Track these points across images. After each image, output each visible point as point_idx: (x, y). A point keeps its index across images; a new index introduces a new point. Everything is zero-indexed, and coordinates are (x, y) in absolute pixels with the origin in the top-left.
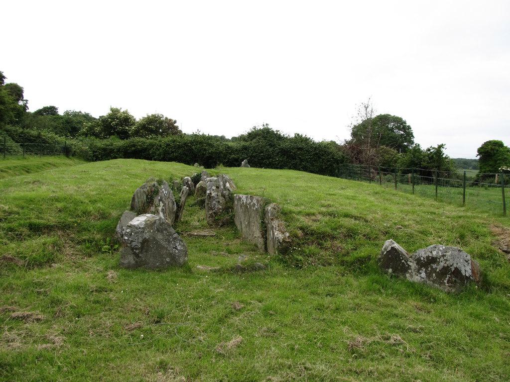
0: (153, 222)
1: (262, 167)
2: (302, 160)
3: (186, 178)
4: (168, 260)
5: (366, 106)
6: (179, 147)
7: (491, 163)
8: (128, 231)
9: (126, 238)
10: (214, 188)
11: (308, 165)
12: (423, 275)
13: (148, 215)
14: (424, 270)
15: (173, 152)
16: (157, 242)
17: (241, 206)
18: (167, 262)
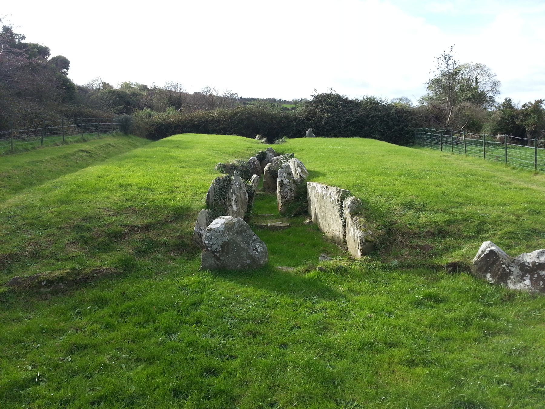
3: (251, 158)
4: (248, 262)
8: (208, 234)
9: (207, 242)
10: (286, 175)
12: (527, 282)
13: (226, 217)
14: (529, 276)
16: (237, 244)
18: (248, 264)
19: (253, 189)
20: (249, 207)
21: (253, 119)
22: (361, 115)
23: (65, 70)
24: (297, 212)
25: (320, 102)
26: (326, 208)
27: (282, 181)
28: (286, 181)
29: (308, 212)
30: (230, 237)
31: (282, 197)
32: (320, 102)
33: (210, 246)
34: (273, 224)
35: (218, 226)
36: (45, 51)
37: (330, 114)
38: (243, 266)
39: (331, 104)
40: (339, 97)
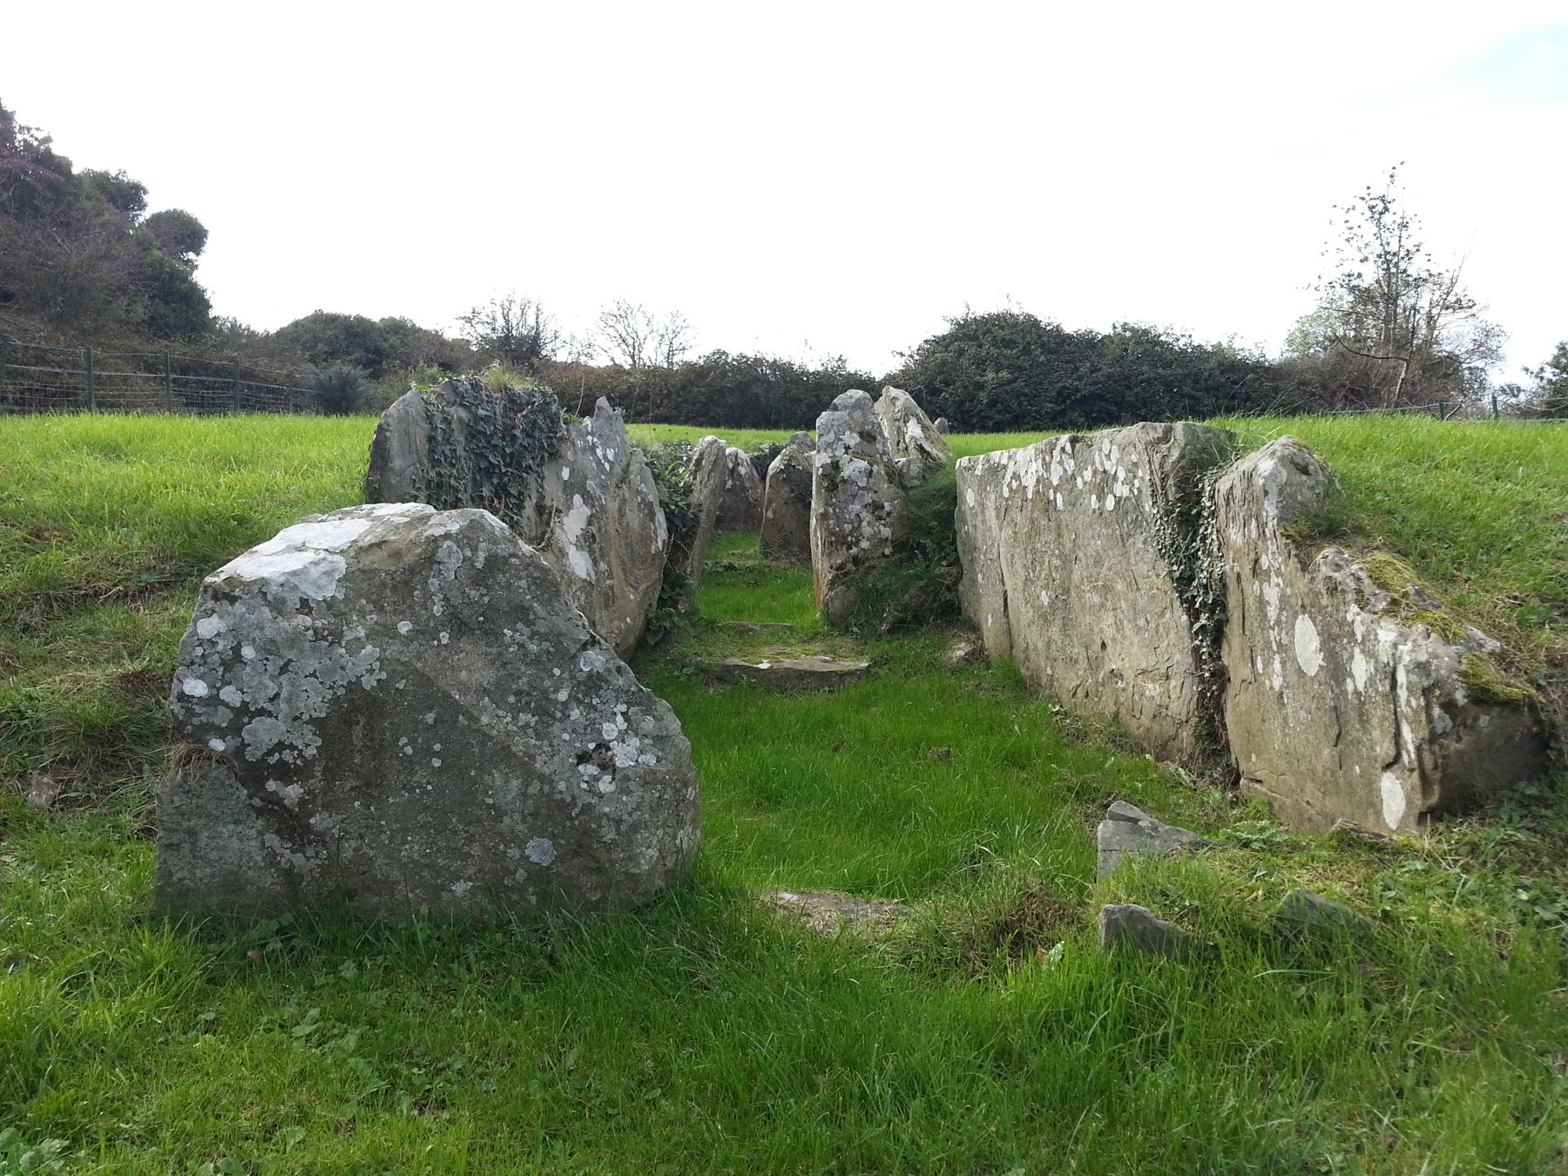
0: (409, 559)
4: (539, 851)
9: (196, 687)
10: (852, 439)
16: (450, 708)
17: (1004, 511)
18: (539, 875)
19: (695, 497)
20: (672, 584)
21: (757, 389)
22: (1109, 376)
23: (191, 255)
24: (905, 609)
25: (975, 338)
26: (1067, 562)
27: (835, 466)
28: (853, 468)
29: (958, 611)
30: (393, 649)
31: (837, 541)
32: (975, 338)
33: (222, 718)
34: (787, 663)
35: (296, 562)
36: (127, 195)
37: (1004, 374)
38: (493, 888)
39: (1008, 344)
40: (1032, 324)
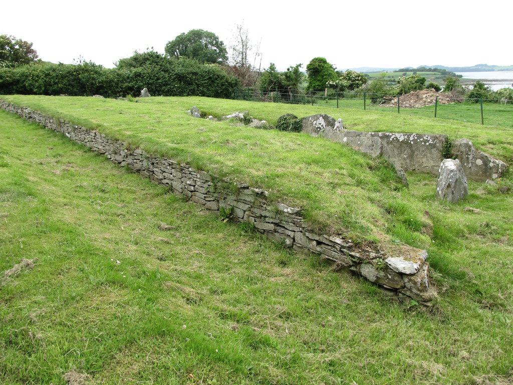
1: (160, 95)
2: (198, 86)
5: (239, 27)
6: (63, 77)
7: (318, 79)
11: (205, 90)
15: (55, 83)
